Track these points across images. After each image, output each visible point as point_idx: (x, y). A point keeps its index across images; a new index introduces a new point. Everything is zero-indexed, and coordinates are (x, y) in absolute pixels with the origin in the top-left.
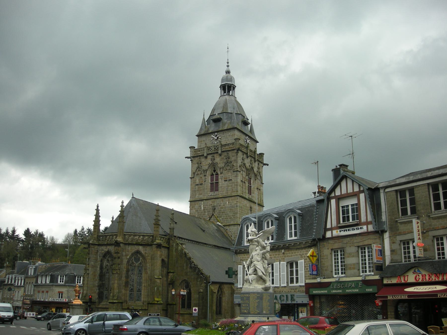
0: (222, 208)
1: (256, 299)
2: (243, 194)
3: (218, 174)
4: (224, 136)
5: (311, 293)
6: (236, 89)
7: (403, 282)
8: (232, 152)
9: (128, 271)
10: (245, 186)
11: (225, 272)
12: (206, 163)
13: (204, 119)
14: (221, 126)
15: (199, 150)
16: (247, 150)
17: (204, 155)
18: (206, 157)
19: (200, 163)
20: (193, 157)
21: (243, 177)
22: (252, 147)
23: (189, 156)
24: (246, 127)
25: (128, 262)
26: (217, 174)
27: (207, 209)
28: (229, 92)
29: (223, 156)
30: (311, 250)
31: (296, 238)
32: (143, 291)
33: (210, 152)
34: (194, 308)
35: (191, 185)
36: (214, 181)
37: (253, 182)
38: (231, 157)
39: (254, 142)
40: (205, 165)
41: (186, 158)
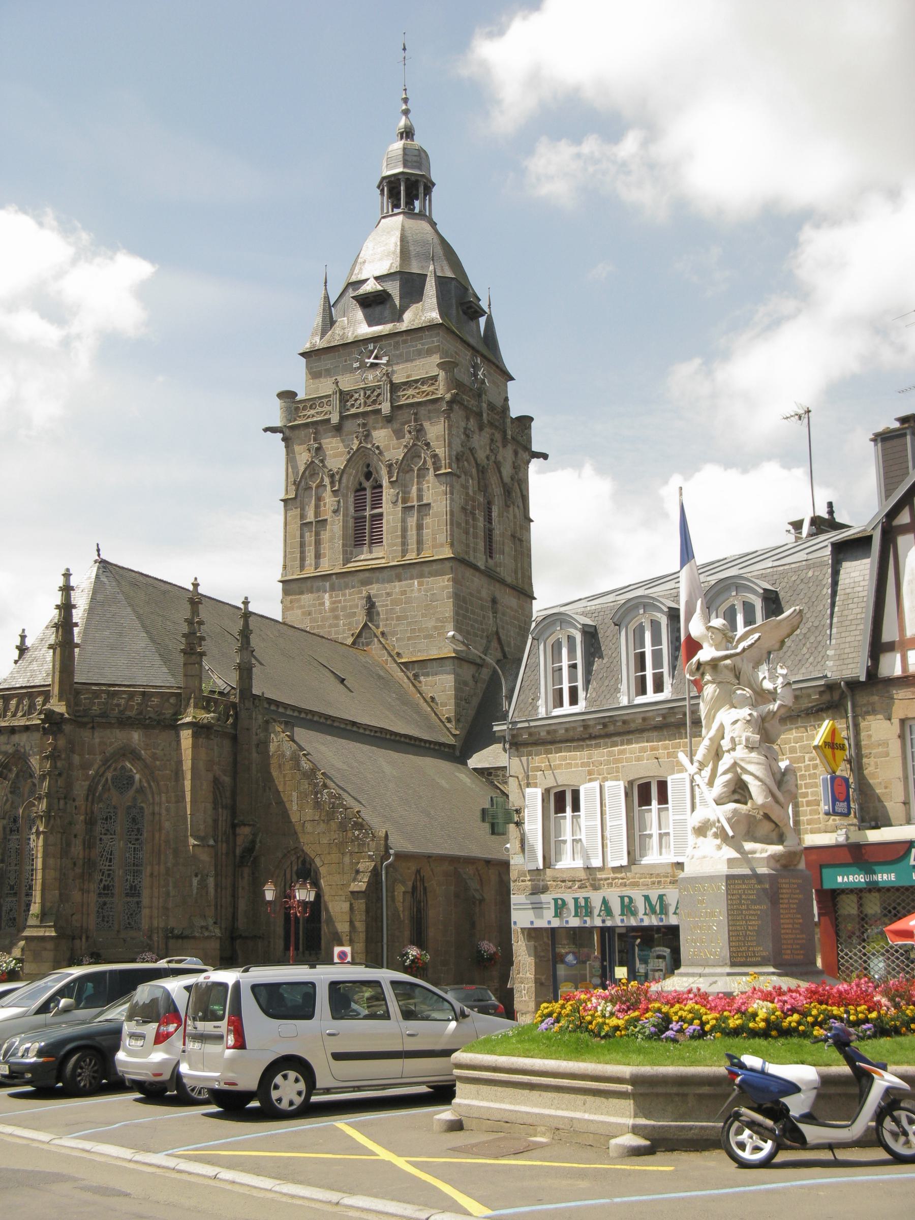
0: (395, 602)
1: (754, 902)
2: (467, 553)
3: (381, 486)
4: (401, 355)
5: (827, 885)
6: (435, 191)
8: (430, 407)
9: (90, 822)
10: (475, 527)
11: (478, 814)
13: (327, 298)
16: (480, 402)
17: (329, 420)
21: (467, 494)
22: (492, 395)
23: (278, 423)
24: (473, 324)
25: (91, 790)
27: (344, 608)
28: (410, 203)
30: (826, 725)
31: (660, 697)
32: (145, 893)
34: (337, 950)
37: (500, 515)
39: (499, 378)
40: (335, 456)
41: (266, 430)
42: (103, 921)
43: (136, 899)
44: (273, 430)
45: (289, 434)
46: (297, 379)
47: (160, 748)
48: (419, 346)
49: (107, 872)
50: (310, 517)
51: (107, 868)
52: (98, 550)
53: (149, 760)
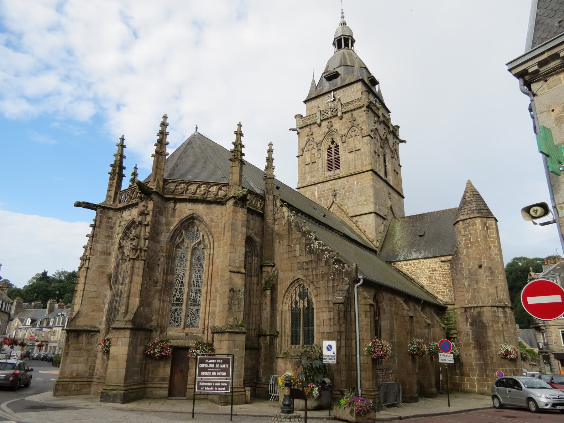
3: (338, 146)
4: (345, 95)
7: (188, 386)
12: (319, 133)
13: (313, 81)
14: (338, 82)
15: (308, 117)
18: (320, 125)
19: (312, 135)
20: (300, 128)
23: (295, 127)
26: (337, 146)
27: (324, 197)
29: (344, 120)
32: (202, 304)
33: (326, 117)
35: (299, 166)
36: (333, 156)
38: (357, 118)
41: (290, 130)
42: (174, 321)
43: (196, 308)
44: (293, 130)
45: (299, 130)
46: (303, 110)
47: (215, 215)
48: (353, 90)
49: (179, 290)
50: (308, 161)
51: (179, 287)
52: (197, 128)
53: (208, 222)
